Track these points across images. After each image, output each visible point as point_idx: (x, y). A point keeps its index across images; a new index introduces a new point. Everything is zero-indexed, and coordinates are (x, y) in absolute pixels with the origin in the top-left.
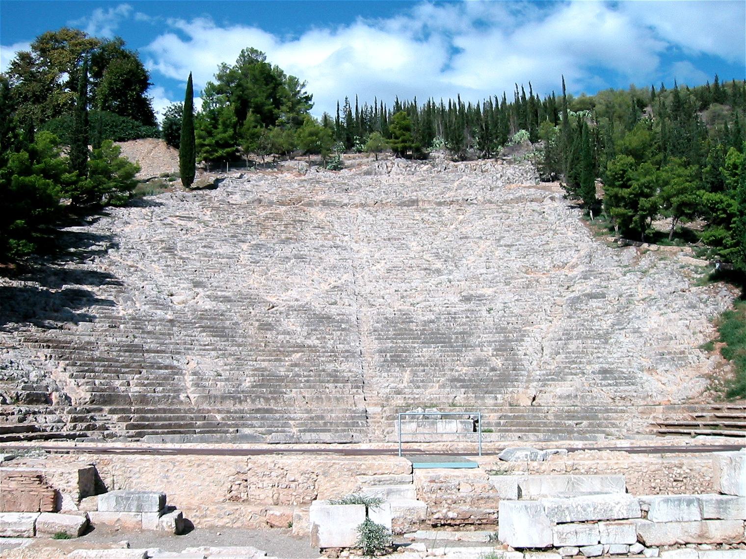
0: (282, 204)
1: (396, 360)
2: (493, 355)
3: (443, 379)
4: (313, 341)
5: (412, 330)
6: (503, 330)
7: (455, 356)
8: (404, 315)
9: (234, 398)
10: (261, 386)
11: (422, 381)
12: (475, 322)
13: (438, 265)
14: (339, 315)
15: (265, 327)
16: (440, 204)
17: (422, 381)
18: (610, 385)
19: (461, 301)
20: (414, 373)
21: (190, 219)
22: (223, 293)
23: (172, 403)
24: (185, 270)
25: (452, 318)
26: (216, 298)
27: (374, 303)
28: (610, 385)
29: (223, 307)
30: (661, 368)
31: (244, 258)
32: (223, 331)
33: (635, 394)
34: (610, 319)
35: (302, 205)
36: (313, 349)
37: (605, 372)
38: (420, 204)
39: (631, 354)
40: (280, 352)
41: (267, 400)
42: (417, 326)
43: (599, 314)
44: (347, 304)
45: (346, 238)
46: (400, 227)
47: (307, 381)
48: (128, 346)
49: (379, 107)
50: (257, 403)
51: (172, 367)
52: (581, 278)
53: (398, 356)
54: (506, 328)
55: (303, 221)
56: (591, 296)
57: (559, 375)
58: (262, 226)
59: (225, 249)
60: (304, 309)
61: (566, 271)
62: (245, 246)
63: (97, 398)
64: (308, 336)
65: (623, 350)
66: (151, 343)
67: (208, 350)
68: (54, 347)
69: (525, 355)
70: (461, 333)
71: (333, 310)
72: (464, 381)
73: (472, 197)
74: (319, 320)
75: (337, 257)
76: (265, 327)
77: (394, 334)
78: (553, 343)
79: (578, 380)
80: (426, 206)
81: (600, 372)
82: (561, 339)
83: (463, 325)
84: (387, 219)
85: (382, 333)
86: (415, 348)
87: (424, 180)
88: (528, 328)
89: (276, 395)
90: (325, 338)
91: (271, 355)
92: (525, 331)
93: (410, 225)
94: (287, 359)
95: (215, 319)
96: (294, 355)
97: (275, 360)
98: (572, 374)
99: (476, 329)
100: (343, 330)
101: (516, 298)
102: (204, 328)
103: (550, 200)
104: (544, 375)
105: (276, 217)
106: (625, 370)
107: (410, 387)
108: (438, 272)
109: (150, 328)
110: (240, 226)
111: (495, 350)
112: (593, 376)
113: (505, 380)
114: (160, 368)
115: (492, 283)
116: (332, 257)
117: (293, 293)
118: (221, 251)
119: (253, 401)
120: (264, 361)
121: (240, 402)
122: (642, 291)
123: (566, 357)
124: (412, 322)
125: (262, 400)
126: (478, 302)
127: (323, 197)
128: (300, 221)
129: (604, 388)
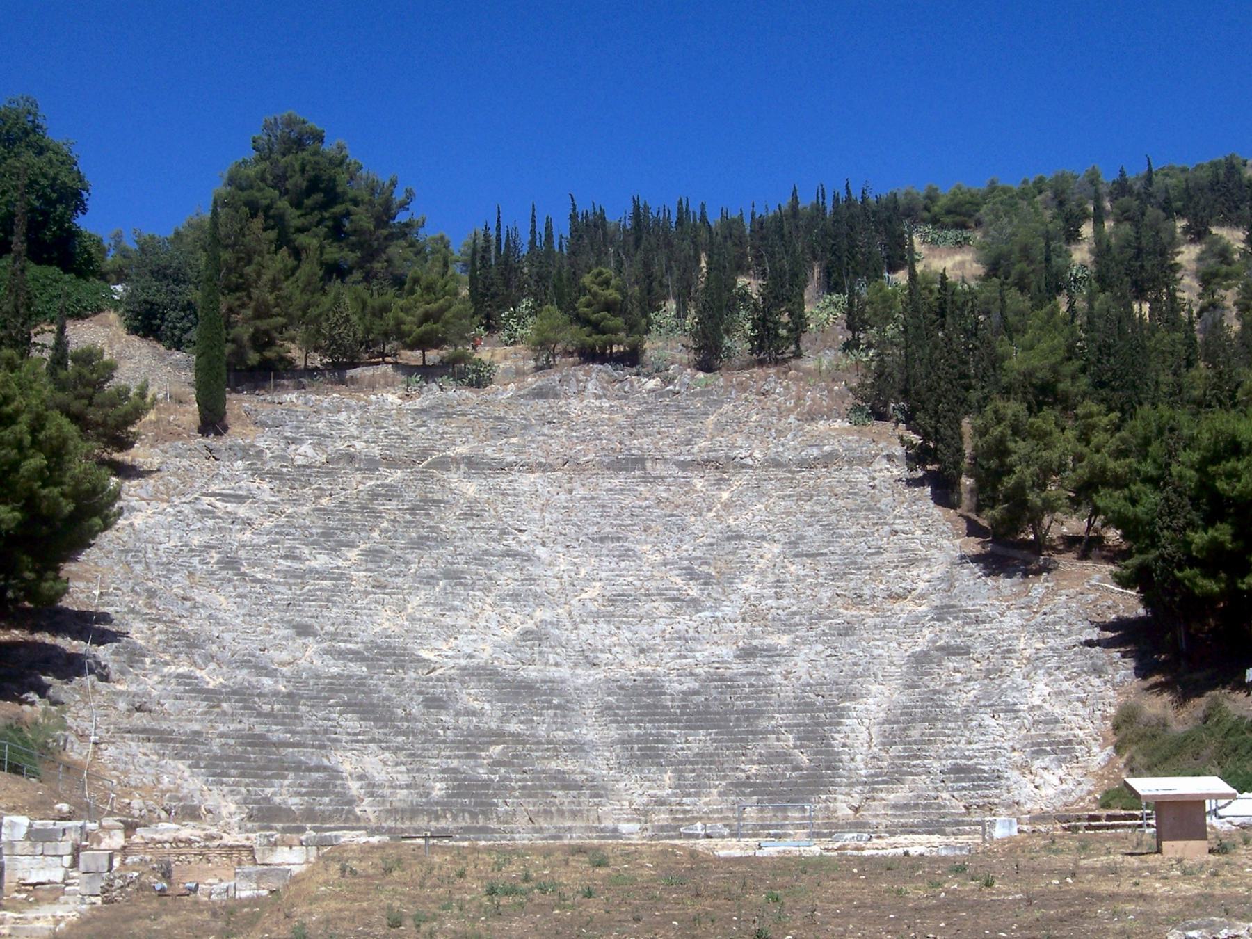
0: (391, 463)
1: (645, 754)
2: (795, 747)
3: (724, 783)
4: (514, 727)
5: (665, 707)
6: (808, 707)
7: (737, 748)
8: (649, 681)
9: (429, 813)
10: (459, 795)
11: (693, 786)
12: (763, 694)
13: (694, 592)
14: (544, 682)
15: (434, 703)
16: (683, 466)
17: (693, 786)
18: (964, 788)
19: (737, 657)
20: (680, 775)
21: (240, 499)
22: (349, 646)
23: (346, 820)
24: (270, 604)
25: (728, 686)
26: (341, 655)
27: (596, 661)
28: (964, 788)
29: (360, 669)
30: (1037, 764)
31: (359, 576)
32: (373, 712)
33: (997, 801)
34: (975, 689)
35: (429, 466)
36: (517, 738)
37: (958, 771)
38: (649, 465)
39: (998, 744)
40: (471, 743)
41: (474, 816)
42: (673, 700)
43: (958, 681)
44: (552, 661)
45: (524, 537)
46: (617, 516)
47: (523, 788)
48: (249, 737)
49: (541, 228)
50: (460, 819)
51: (325, 769)
52: (933, 619)
53: (650, 749)
54: (813, 704)
55: (440, 501)
56: (950, 651)
57: (895, 776)
58: (368, 509)
59: (321, 561)
60: (484, 674)
61: (908, 605)
62: (353, 554)
63: (255, 812)
64: (504, 719)
65: (994, 739)
66: (278, 733)
67: (361, 741)
68: (156, 741)
69: (844, 745)
70: (743, 712)
71: (532, 673)
72: (754, 785)
73: (744, 453)
74: (515, 691)
75: (518, 575)
76: (434, 703)
77: (639, 714)
78: (886, 727)
79: (922, 781)
80: (660, 470)
81: (951, 771)
82: (897, 722)
83: (746, 698)
84: (593, 498)
85: (620, 712)
86: (674, 735)
87: (650, 411)
88: (848, 704)
89: (486, 808)
90: (532, 721)
91: (458, 749)
92: (843, 709)
93: (637, 511)
94: (483, 754)
95: (353, 691)
96: (491, 749)
97: (468, 756)
98: (911, 774)
99: (766, 705)
100: (557, 707)
101: (829, 651)
102: (349, 706)
103: (885, 461)
104: (872, 775)
105: (391, 493)
106: (986, 768)
107: (675, 795)
108: (695, 604)
109: (266, 708)
110: (332, 513)
111: (799, 739)
112: (942, 776)
113: (816, 784)
114: (309, 769)
115: (787, 626)
116: (508, 578)
117: (464, 643)
118: (313, 564)
119: (455, 817)
120: (449, 757)
121: (437, 819)
122: (1027, 645)
123: (905, 750)
124: (665, 694)
125: (466, 815)
126: (766, 660)
127: (463, 450)
128: (434, 501)
129: (955, 794)
